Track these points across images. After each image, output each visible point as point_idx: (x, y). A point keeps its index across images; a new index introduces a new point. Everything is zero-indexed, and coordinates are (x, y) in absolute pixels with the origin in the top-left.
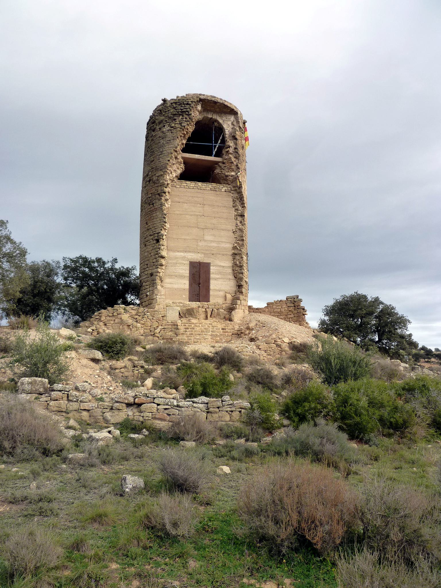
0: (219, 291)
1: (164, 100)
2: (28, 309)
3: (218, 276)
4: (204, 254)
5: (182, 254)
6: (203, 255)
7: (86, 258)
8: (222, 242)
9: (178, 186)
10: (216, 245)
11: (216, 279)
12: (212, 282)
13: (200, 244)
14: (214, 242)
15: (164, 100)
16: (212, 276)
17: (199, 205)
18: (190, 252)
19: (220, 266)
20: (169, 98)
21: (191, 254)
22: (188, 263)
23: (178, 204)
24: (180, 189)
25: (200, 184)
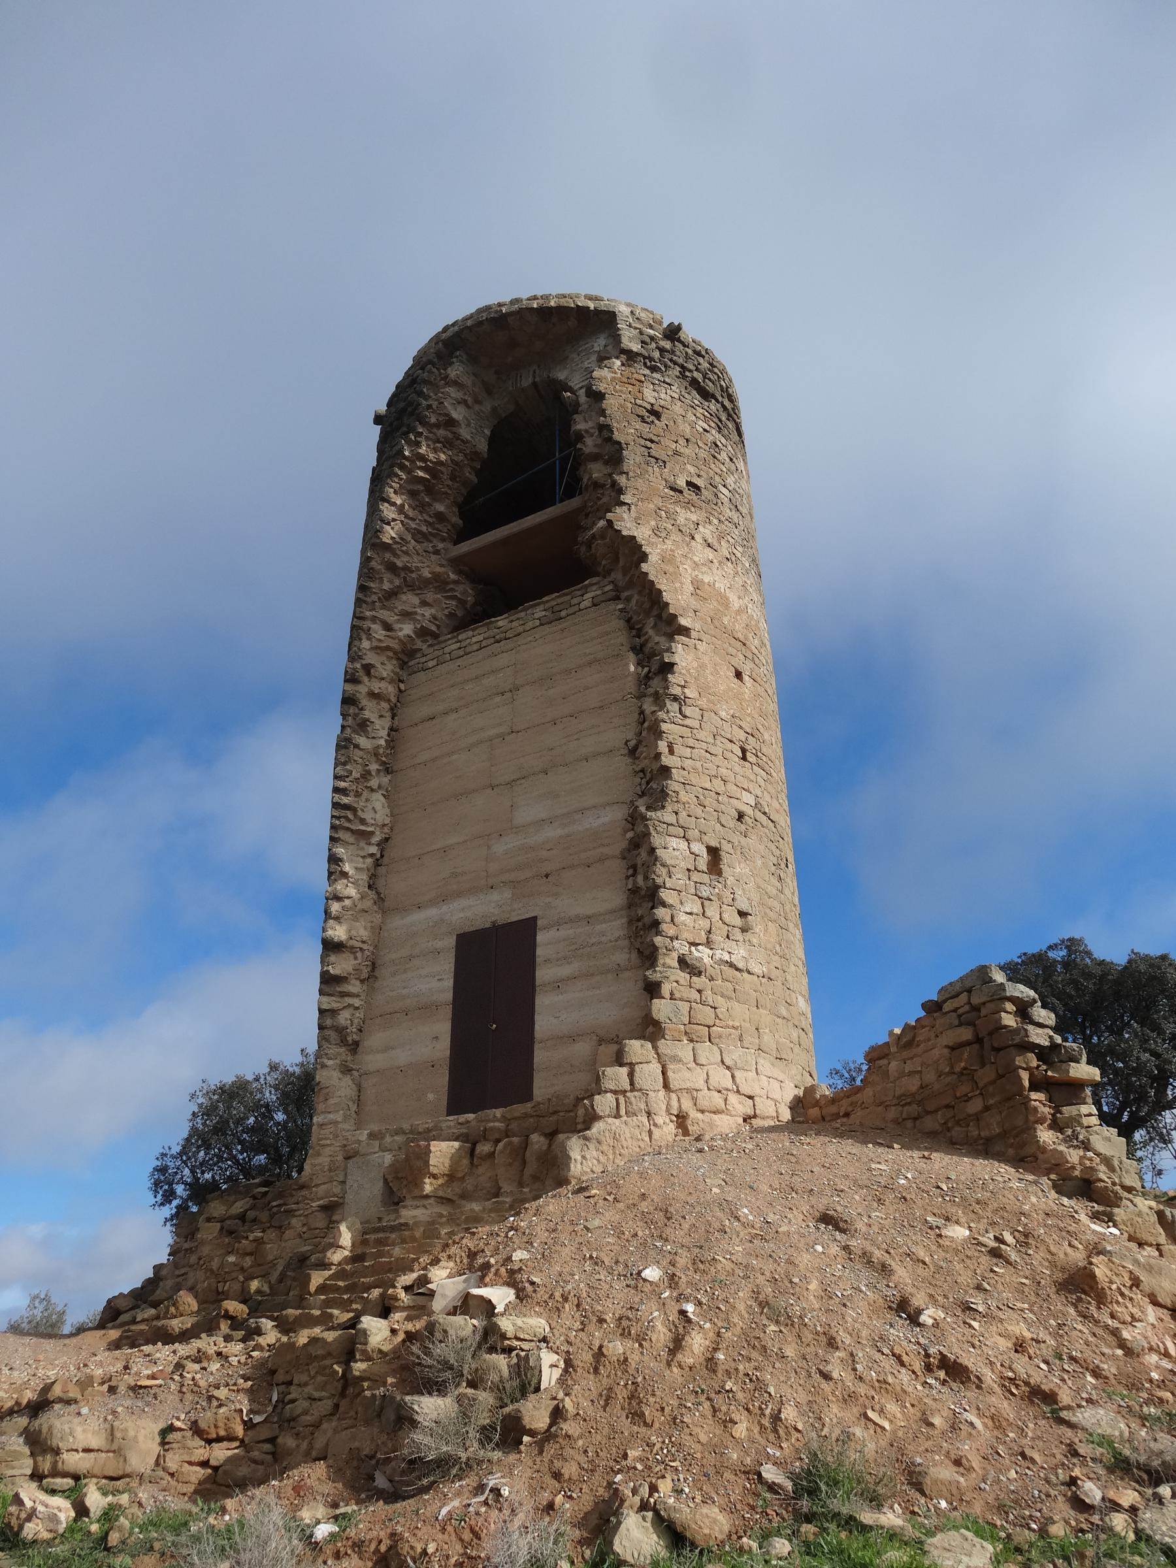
0: (573, 1038)
1: (378, 419)
2: (444, 1219)
3: (566, 971)
4: (513, 884)
5: (432, 912)
6: (507, 894)
7: (1038, 959)
8: (582, 811)
9: (431, 664)
10: (559, 832)
11: (557, 985)
12: (542, 1001)
13: (499, 848)
14: (551, 821)
15: (378, 419)
16: (543, 974)
17: (498, 699)
18: (459, 894)
19: (577, 919)
20: (689, 332)
21: (463, 902)
22: (451, 941)
23: (454, 716)
24: (442, 668)
25: (502, 622)
